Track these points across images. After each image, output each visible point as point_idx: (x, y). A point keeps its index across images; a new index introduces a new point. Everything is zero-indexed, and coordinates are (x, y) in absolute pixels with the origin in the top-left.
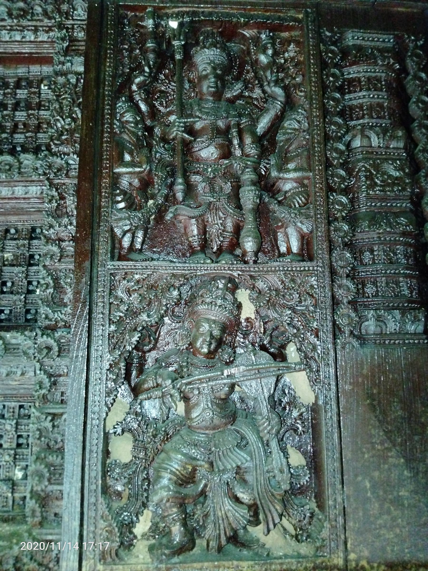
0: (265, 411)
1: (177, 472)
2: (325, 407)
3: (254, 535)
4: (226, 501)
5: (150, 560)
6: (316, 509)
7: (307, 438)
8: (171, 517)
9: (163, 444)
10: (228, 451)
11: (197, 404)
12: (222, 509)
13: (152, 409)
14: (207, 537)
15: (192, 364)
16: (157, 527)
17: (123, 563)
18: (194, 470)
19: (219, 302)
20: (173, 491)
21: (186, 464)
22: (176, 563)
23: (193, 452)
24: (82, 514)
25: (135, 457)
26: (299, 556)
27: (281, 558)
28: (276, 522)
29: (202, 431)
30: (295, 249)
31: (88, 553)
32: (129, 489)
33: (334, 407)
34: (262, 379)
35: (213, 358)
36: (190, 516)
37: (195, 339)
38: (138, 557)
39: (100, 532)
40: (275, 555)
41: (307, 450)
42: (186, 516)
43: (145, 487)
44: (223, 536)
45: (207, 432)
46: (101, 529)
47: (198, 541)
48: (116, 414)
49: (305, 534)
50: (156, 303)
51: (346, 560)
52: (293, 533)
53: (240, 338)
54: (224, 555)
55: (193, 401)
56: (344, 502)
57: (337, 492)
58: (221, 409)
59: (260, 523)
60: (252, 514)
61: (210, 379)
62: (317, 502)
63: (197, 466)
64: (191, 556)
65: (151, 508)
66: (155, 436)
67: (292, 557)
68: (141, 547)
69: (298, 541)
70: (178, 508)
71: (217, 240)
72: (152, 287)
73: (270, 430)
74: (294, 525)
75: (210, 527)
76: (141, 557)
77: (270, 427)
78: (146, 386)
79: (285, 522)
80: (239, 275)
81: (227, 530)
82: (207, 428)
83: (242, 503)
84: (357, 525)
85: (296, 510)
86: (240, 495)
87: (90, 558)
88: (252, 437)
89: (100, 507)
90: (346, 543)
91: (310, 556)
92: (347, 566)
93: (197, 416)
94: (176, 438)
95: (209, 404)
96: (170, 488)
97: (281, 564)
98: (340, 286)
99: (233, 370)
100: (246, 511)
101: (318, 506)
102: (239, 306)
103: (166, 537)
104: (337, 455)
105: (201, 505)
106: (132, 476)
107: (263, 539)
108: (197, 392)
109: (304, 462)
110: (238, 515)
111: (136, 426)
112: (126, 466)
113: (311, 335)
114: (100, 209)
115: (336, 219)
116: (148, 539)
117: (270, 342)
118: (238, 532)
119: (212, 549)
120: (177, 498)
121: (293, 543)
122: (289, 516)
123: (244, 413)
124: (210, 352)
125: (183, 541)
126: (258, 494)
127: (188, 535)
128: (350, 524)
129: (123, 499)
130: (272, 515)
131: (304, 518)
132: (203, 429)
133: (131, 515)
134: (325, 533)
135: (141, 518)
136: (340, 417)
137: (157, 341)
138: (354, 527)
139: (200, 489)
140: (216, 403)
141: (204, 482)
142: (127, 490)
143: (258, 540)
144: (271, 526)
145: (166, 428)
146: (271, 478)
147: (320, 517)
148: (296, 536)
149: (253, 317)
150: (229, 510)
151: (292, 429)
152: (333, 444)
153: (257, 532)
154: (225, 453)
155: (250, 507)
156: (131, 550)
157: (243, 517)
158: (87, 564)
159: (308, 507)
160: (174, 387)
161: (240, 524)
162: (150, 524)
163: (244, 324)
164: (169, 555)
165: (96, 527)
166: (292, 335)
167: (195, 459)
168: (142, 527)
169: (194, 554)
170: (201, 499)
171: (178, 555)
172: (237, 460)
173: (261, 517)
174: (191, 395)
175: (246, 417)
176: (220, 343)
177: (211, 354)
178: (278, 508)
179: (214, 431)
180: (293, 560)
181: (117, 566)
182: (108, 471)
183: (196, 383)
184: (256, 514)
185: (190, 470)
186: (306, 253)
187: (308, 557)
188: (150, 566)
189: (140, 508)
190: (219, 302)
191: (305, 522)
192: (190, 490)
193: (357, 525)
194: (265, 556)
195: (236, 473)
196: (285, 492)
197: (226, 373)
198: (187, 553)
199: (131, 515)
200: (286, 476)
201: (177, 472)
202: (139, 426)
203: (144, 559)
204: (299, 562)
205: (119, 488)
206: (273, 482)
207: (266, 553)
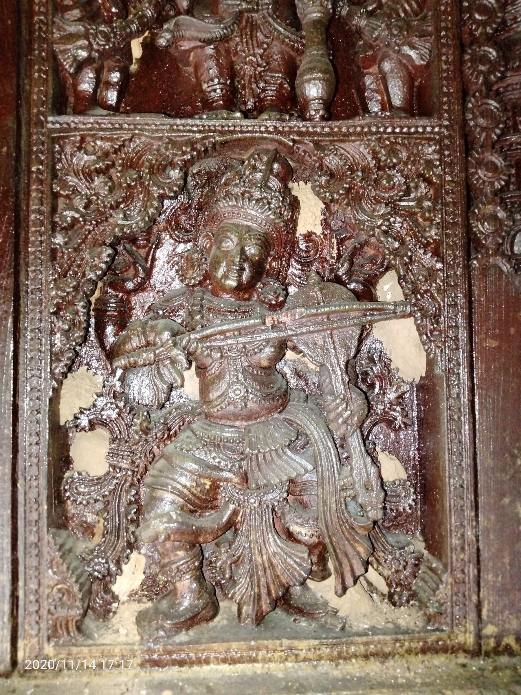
0: (340, 387)
1: (186, 491)
2: (448, 379)
3: (319, 595)
4: (271, 537)
5: (138, 638)
6: (425, 552)
7: (409, 437)
8: (174, 567)
9: (162, 445)
10: (273, 454)
11: (219, 377)
12: (264, 552)
13: (142, 388)
14: (238, 597)
15: (209, 309)
16: (154, 581)
17: (90, 642)
18: (215, 487)
19: (257, 195)
20: (176, 521)
21: (200, 476)
22: (181, 644)
23: (212, 458)
24: (15, 562)
25: (114, 467)
26: (398, 630)
27: (365, 634)
28: (358, 573)
29: (228, 423)
30: (397, 101)
31: (27, 627)
32: (105, 519)
33: (464, 376)
34: (335, 332)
35: (249, 299)
36: (211, 562)
37: (215, 264)
38: (118, 631)
39: (47, 591)
40: (355, 629)
41: (409, 456)
42: (202, 563)
43: (132, 516)
44: (264, 596)
45: (237, 423)
46: (48, 587)
47: (223, 604)
48: (79, 396)
49: (406, 593)
50: (141, 196)
51: (479, 636)
52: (385, 590)
53: (295, 269)
54: (266, 628)
55: (214, 370)
56: (478, 541)
57: (466, 523)
58: (262, 384)
59: (330, 575)
60: (315, 559)
61: (240, 332)
62: (426, 541)
63: (220, 480)
64: (209, 630)
65: (143, 551)
66: (146, 431)
67: (385, 632)
68: (127, 614)
69: (394, 604)
70: (186, 550)
71: (254, 86)
72: (131, 164)
73: (347, 418)
74: (386, 579)
75: (243, 582)
76: (123, 631)
77: (348, 413)
78: (128, 346)
79: (372, 574)
80: (294, 141)
81: (272, 586)
82: (236, 417)
83: (298, 542)
84: (500, 579)
85: (391, 553)
86: (294, 528)
87: (31, 636)
88: (315, 431)
89: (45, 549)
90: (479, 607)
91: (417, 629)
92: (480, 645)
93: (219, 397)
94: (182, 436)
95: (240, 376)
96: (171, 517)
97: (366, 644)
98: (480, 164)
99: (284, 317)
100: (306, 555)
101: (428, 548)
102: (294, 205)
103: (168, 598)
104: (467, 461)
105: (227, 545)
106: (110, 498)
107: (334, 602)
108: (219, 355)
109: (404, 476)
110: (293, 562)
111: (114, 415)
112: (99, 481)
113: (425, 253)
114: (32, 18)
115: (474, 41)
116: (139, 601)
117: (349, 273)
118: (292, 590)
119: (246, 619)
120: (183, 533)
121: (386, 607)
122: (379, 563)
123: (303, 395)
124: (240, 284)
125: (196, 606)
126: (327, 526)
127: (206, 596)
128: (488, 577)
129: (96, 537)
130: (349, 561)
131: (405, 568)
132: (228, 419)
133: (107, 562)
134: (444, 591)
135: (124, 567)
136: (473, 396)
137: (149, 273)
138: (495, 582)
139: (225, 519)
140: (252, 374)
141: (232, 507)
142: (102, 521)
143: (326, 604)
144: (349, 580)
145: (166, 419)
146: (348, 499)
147: (434, 565)
148: (391, 596)
149: (318, 230)
150: (275, 554)
151: (384, 420)
152: (460, 442)
153: (324, 590)
154: (268, 457)
155: (311, 548)
156: (109, 620)
157: (299, 565)
158: (25, 645)
159: (411, 548)
160: (175, 344)
161: (294, 576)
162: (143, 577)
163: (303, 245)
164: (170, 630)
165: (39, 584)
166: (391, 253)
167: (218, 469)
168: (129, 579)
169: (216, 627)
170: (229, 535)
171: (188, 629)
172: (289, 469)
173: (331, 565)
174: (208, 361)
175: (307, 400)
176: (259, 271)
177: (244, 290)
178: (361, 549)
179: (250, 423)
180: (388, 638)
181: (79, 649)
182: (66, 491)
183: (216, 339)
184: (322, 560)
185: (207, 487)
186: (419, 103)
187: (413, 631)
188: (136, 647)
189: (123, 550)
190: (257, 195)
191: (407, 572)
192: (209, 520)
193: (500, 579)
194: (339, 635)
195: (288, 492)
196: (375, 522)
197: (269, 321)
198: (204, 625)
199: (107, 562)
200: (377, 496)
201: (186, 491)
202: (119, 415)
203: (127, 635)
204: (397, 640)
205: (90, 518)
206: (352, 506)
207: (340, 626)
